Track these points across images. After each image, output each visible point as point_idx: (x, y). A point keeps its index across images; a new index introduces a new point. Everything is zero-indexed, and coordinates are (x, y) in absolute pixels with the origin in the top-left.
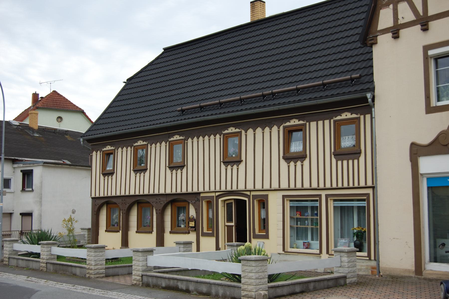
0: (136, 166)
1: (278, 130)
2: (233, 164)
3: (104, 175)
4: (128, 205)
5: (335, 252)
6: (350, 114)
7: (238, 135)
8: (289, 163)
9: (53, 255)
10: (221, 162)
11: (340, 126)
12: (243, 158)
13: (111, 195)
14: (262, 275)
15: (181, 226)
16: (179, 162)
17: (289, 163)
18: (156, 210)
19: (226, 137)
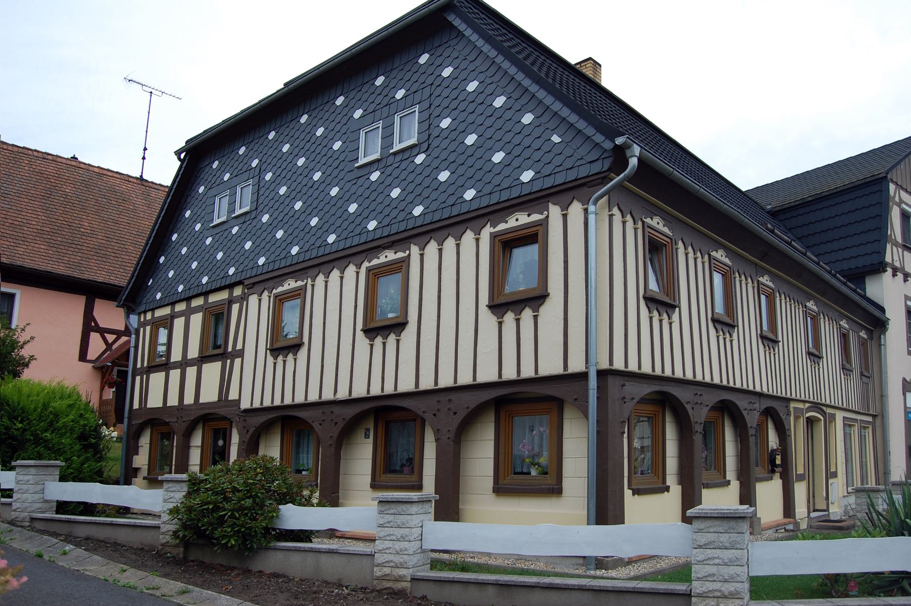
0: (277, 340)
1: (563, 215)
2: (286, 352)
3: (371, 332)
4: (462, 415)
5: (380, 502)
6: (393, 253)
7: (299, 294)
8: (372, 339)
9: (47, 501)
10: (267, 349)
11: (378, 278)
12: (306, 339)
13: (500, 375)
14: (395, 560)
15: (529, 473)
16: (292, 338)
17: (372, 339)
18: (437, 432)
19: (280, 300)
